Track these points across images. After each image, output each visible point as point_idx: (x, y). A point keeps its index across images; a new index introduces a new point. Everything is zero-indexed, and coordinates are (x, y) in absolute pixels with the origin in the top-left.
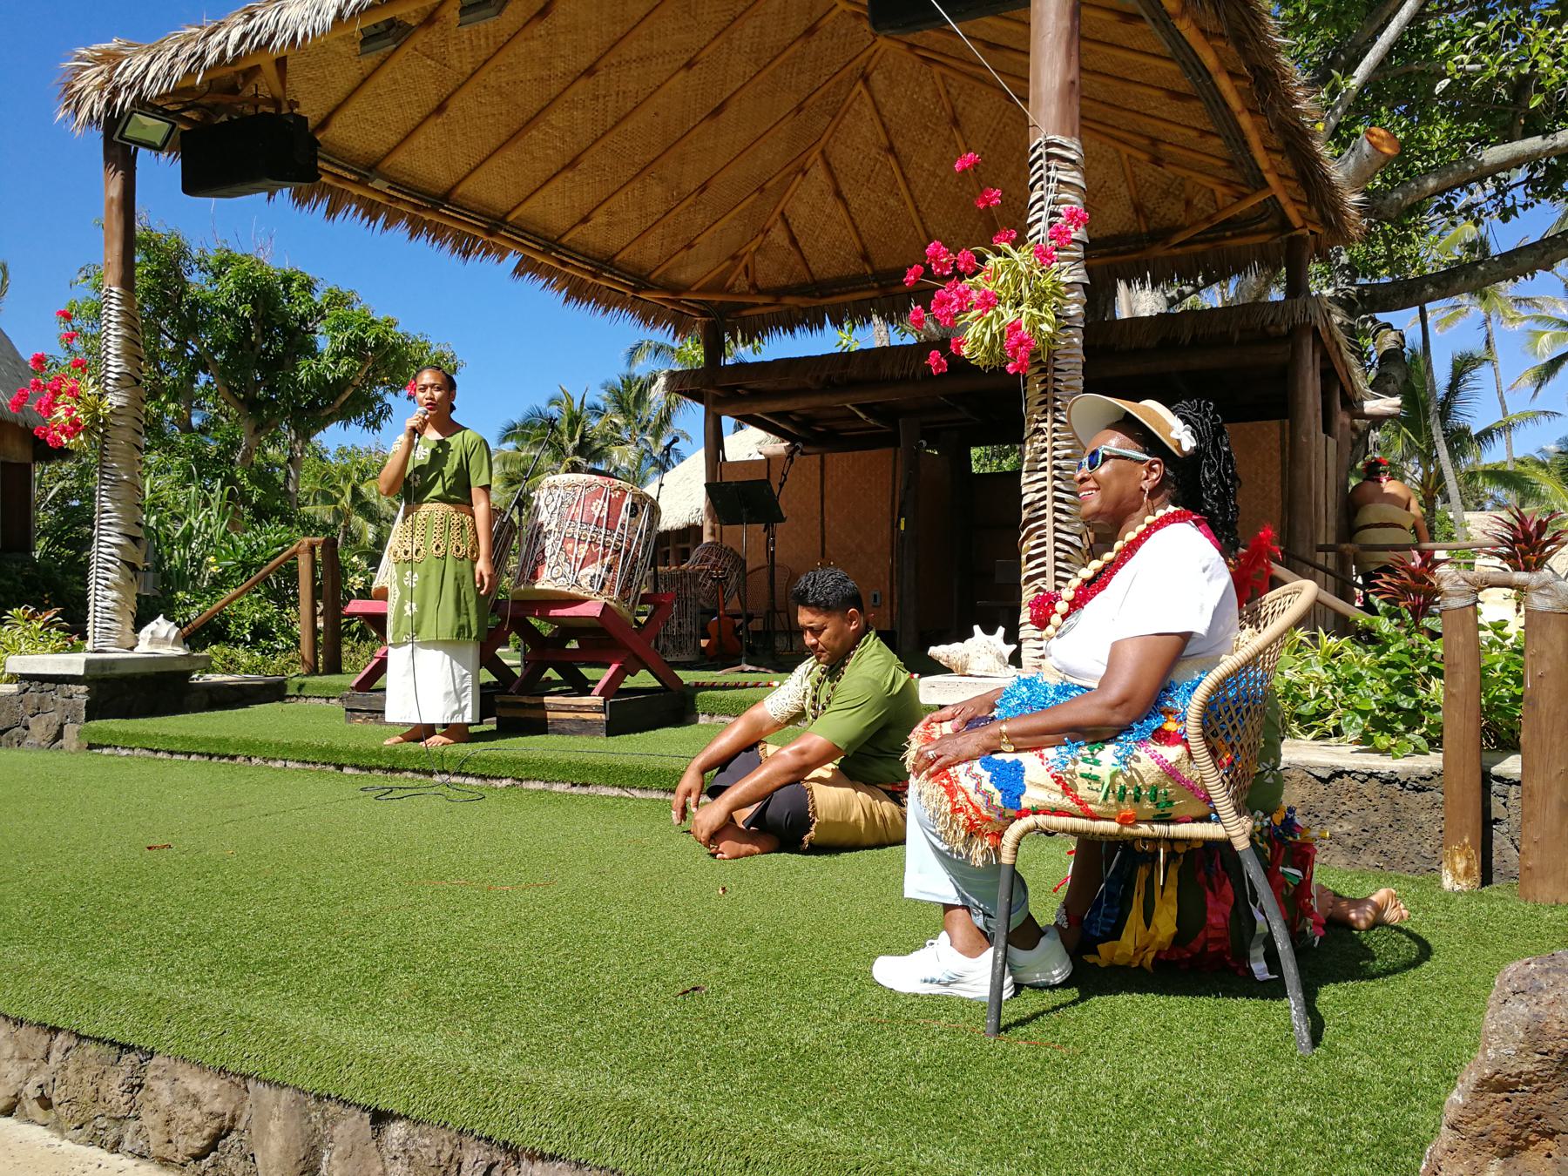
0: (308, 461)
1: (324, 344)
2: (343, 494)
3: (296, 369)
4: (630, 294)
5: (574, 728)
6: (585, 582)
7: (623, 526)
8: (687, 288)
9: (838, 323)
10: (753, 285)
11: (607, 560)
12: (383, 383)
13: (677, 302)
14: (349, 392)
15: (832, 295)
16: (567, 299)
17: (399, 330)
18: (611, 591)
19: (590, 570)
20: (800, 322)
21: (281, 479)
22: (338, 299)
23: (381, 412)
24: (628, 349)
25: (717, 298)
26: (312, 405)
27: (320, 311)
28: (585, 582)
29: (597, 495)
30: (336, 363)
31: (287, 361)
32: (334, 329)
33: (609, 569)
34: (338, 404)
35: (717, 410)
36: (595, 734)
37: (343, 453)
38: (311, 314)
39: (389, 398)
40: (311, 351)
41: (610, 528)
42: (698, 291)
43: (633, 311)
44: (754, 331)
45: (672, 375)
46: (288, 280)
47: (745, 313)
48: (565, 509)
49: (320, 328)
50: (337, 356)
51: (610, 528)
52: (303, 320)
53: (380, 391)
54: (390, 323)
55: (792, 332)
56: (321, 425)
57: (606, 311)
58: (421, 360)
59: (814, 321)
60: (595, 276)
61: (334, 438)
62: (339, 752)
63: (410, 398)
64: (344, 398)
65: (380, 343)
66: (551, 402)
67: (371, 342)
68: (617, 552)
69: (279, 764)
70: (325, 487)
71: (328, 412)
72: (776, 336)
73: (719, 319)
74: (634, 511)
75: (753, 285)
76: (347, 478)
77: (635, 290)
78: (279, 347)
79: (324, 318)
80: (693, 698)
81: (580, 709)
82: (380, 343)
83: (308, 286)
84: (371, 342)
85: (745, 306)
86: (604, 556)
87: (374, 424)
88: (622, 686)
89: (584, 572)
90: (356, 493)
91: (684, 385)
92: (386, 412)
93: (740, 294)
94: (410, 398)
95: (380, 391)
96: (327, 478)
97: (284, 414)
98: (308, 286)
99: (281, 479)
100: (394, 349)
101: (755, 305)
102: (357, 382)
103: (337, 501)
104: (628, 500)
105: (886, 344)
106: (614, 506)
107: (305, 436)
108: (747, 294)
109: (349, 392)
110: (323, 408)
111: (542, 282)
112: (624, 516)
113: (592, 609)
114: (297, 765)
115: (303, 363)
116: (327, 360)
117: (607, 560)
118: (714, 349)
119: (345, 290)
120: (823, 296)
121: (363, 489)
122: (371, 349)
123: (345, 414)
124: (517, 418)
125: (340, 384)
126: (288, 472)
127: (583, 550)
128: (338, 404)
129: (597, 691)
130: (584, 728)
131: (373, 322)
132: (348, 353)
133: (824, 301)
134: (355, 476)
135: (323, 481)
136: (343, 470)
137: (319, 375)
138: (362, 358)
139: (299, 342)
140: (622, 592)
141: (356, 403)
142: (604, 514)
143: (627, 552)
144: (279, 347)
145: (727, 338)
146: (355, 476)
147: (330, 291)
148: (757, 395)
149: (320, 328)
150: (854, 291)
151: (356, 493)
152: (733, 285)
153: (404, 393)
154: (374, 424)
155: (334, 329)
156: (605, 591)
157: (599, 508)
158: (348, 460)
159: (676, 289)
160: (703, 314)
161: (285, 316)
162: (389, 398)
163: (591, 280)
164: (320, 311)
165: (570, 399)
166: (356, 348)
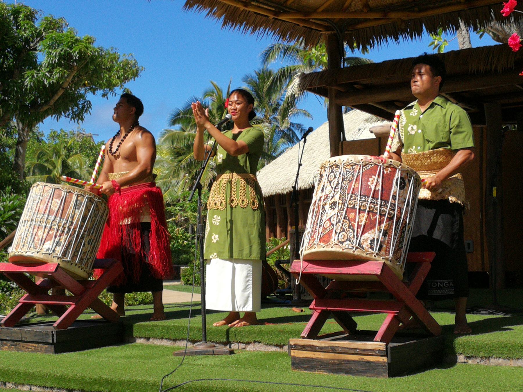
0: (30, 143)
1: (42, 58)
2: (55, 167)
3: (23, 77)
4: (271, 17)
5: (360, 368)
6: (366, 245)
7: (394, 197)
8: (315, 10)
9: (433, 30)
10: (366, 5)
11: (383, 226)
12: (85, 85)
13: (307, 21)
14: (61, 93)
15: (426, 10)
16: (225, 23)
17: (96, 45)
18: (387, 252)
19: (369, 235)
20: (403, 31)
21: (12, 159)
22: (52, 25)
23: (83, 107)
24: (263, 51)
25: (337, 17)
26: (34, 103)
27: (39, 34)
28: (366, 245)
29: (372, 172)
30: (50, 72)
31: (16, 72)
32: (50, 47)
33: (385, 233)
34: (52, 102)
35: (338, 102)
36: (378, 374)
37: (54, 136)
38: (32, 36)
39: (89, 96)
40: (34, 65)
41: (385, 200)
42: (323, 12)
43: (273, 29)
44: (365, 42)
45: (304, 77)
46: (16, 12)
47: (360, 26)
48: (346, 184)
49: (40, 46)
50: (52, 67)
51: (385, 200)
52: (27, 41)
53: (82, 91)
54: (89, 41)
55: (396, 38)
56: (40, 118)
57: (254, 30)
58: (112, 67)
59: (414, 30)
60: (246, 5)
61: (48, 126)
62: (70, 380)
63: (104, 95)
64: (56, 97)
65: (82, 56)
66: (206, 94)
67: (76, 56)
68: (390, 219)
69: (26, 388)
70: (41, 162)
71: (45, 108)
72: (384, 43)
73: (339, 33)
74: (403, 185)
75: (366, 5)
76: (58, 154)
77: (276, 13)
78: (10, 62)
79: (42, 39)
80: (131, 329)
81: (364, 352)
82: (82, 56)
83: (30, 16)
84: (76, 56)
85: (360, 21)
86: (380, 223)
87: (78, 116)
88: (78, 319)
89: (366, 235)
90: (65, 165)
91: (312, 84)
92: (87, 107)
93: (355, 12)
94: (104, 95)
95: (82, 91)
96: (41, 155)
97: (14, 111)
98: (30, 16)
99: (12, 159)
100: (93, 59)
101: (366, 20)
102: (66, 85)
103: (50, 172)
104: (398, 175)
105: (466, 46)
106: (387, 180)
107: (30, 125)
108: (361, 12)
109: (61, 93)
110: (42, 105)
111: (206, 12)
112: (395, 189)
113: (373, 268)
114: (39, 389)
115: (28, 73)
116: (44, 70)
117: (383, 226)
118: (336, 53)
119: (57, 18)
120: (420, 11)
121: (70, 162)
122: (75, 61)
123: (57, 110)
124: (181, 106)
125: (54, 88)
126: (17, 150)
127: (363, 219)
128: (52, 102)
129: (378, 337)
130: (367, 369)
131: (77, 40)
132: (59, 65)
133: (421, 15)
134: (63, 152)
135: (39, 158)
136: (55, 149)
137: (39, 81)
138: (69, 67)
139: (25, 58)
140: (395, 252)
141: (64, 100)
142: (379, 187)
143: (399, 219)
144: (10, 62)
145: (345, 45)
146: (63, 152)
147: (46, 19)
148: (369, 89)
149: (40, 46)
150: (444, 6)
151: (65, 165)
152: (350, 5)
153: (100, 92)
154: (78, 116)
155: (50, 47)
156: (383, 252)
157: (375, 183)
158: (57, 141)
159: (306, 11)
160: (327, 28)
161: (14, 39)
162: (89, 96)
163: (242, 8)
164: (39, 34)
165: (219, 90)
166: (65, 60)
